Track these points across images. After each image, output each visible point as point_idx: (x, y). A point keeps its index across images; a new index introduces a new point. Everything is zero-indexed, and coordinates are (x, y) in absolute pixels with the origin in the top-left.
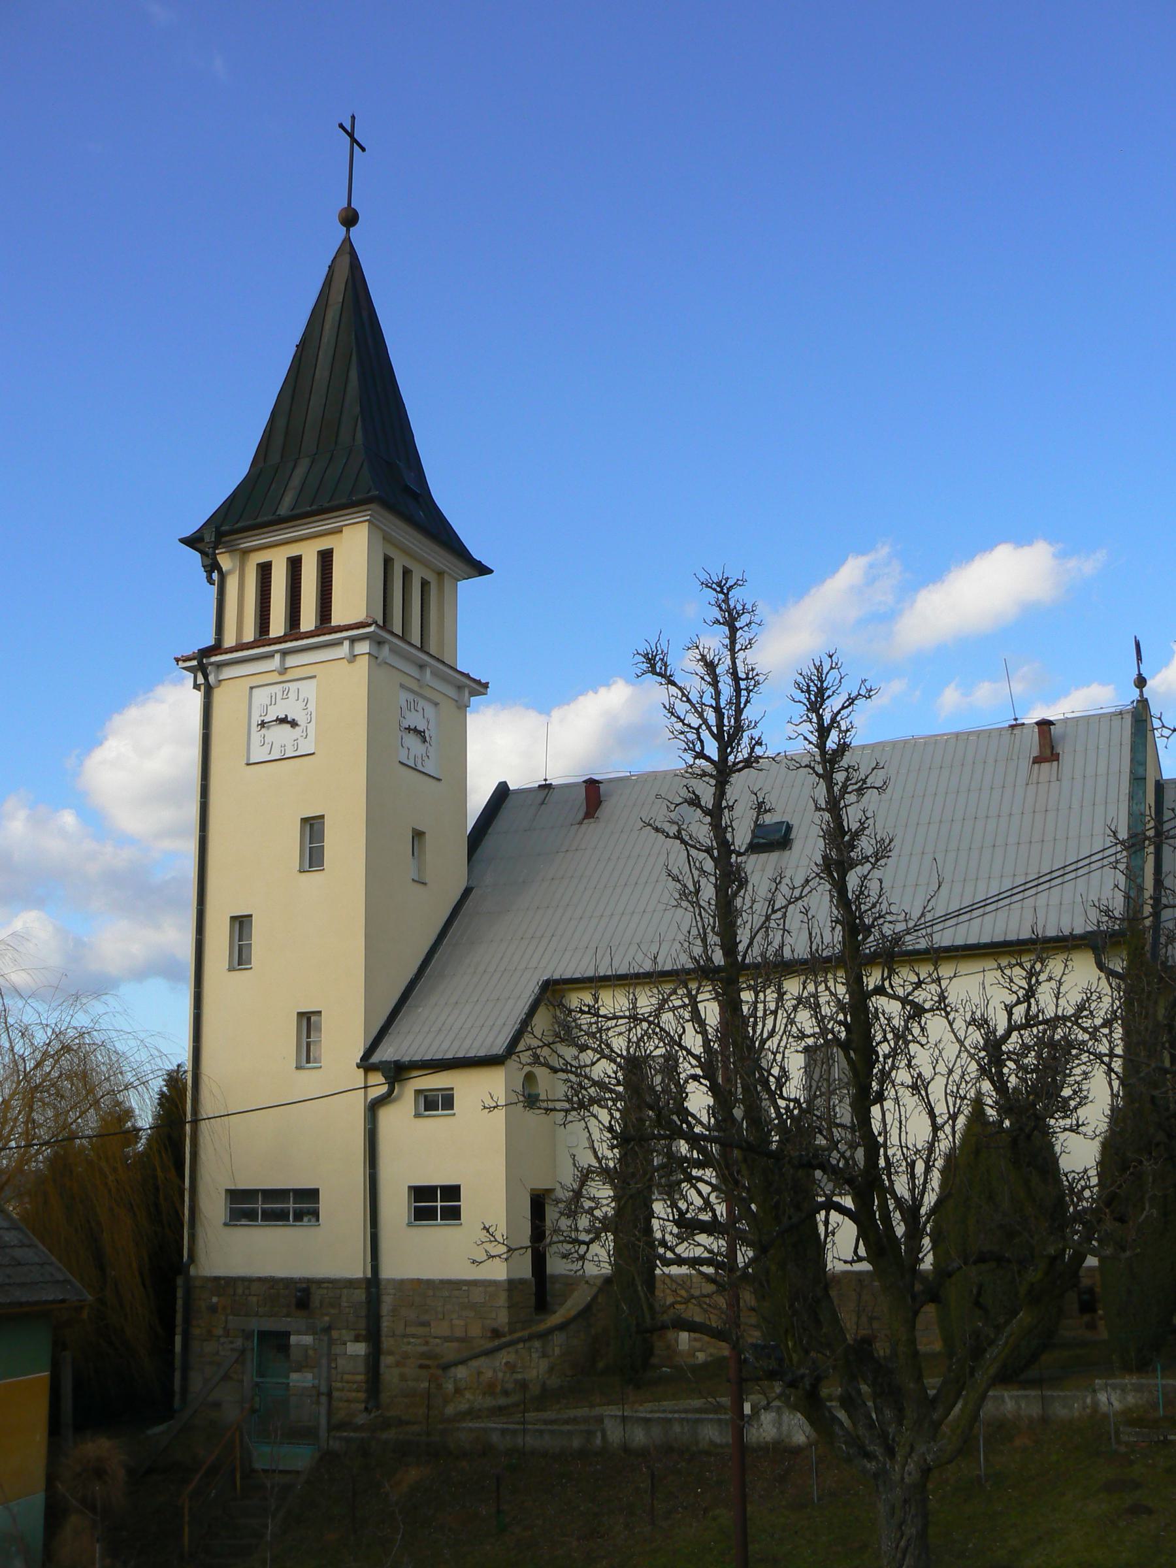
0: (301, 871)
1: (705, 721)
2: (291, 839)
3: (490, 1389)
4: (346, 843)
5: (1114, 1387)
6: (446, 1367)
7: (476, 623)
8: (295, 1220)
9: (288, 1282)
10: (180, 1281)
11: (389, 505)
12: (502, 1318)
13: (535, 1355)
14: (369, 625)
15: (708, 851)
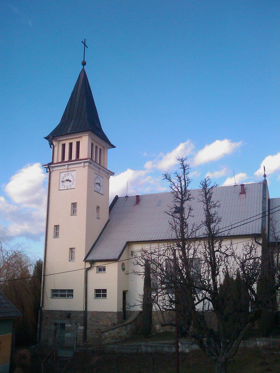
0: (71, 215)
1: (178, 190)
2: (69, 207)
3: (113, 338)
4: (82, 209)
5: (261, 340)
6: (103, 332)
7: (111, 158)
8: (67, 297)
9: (65, 311)
10: (39, 311)
11: (93, 132)
12: (116, 321)
13: (123, 330)
14: (88, 159)
15: (179, 219)
